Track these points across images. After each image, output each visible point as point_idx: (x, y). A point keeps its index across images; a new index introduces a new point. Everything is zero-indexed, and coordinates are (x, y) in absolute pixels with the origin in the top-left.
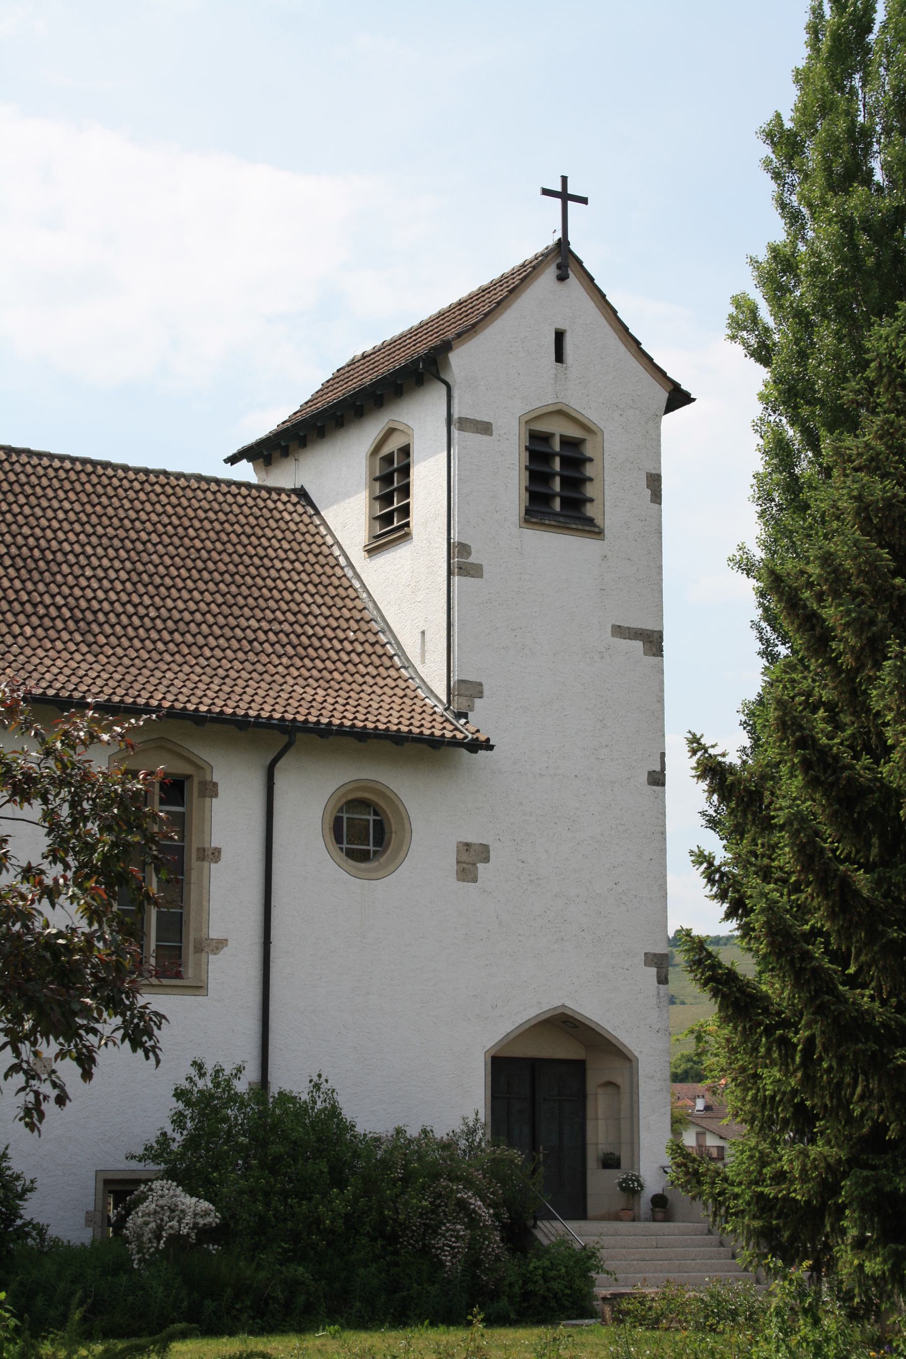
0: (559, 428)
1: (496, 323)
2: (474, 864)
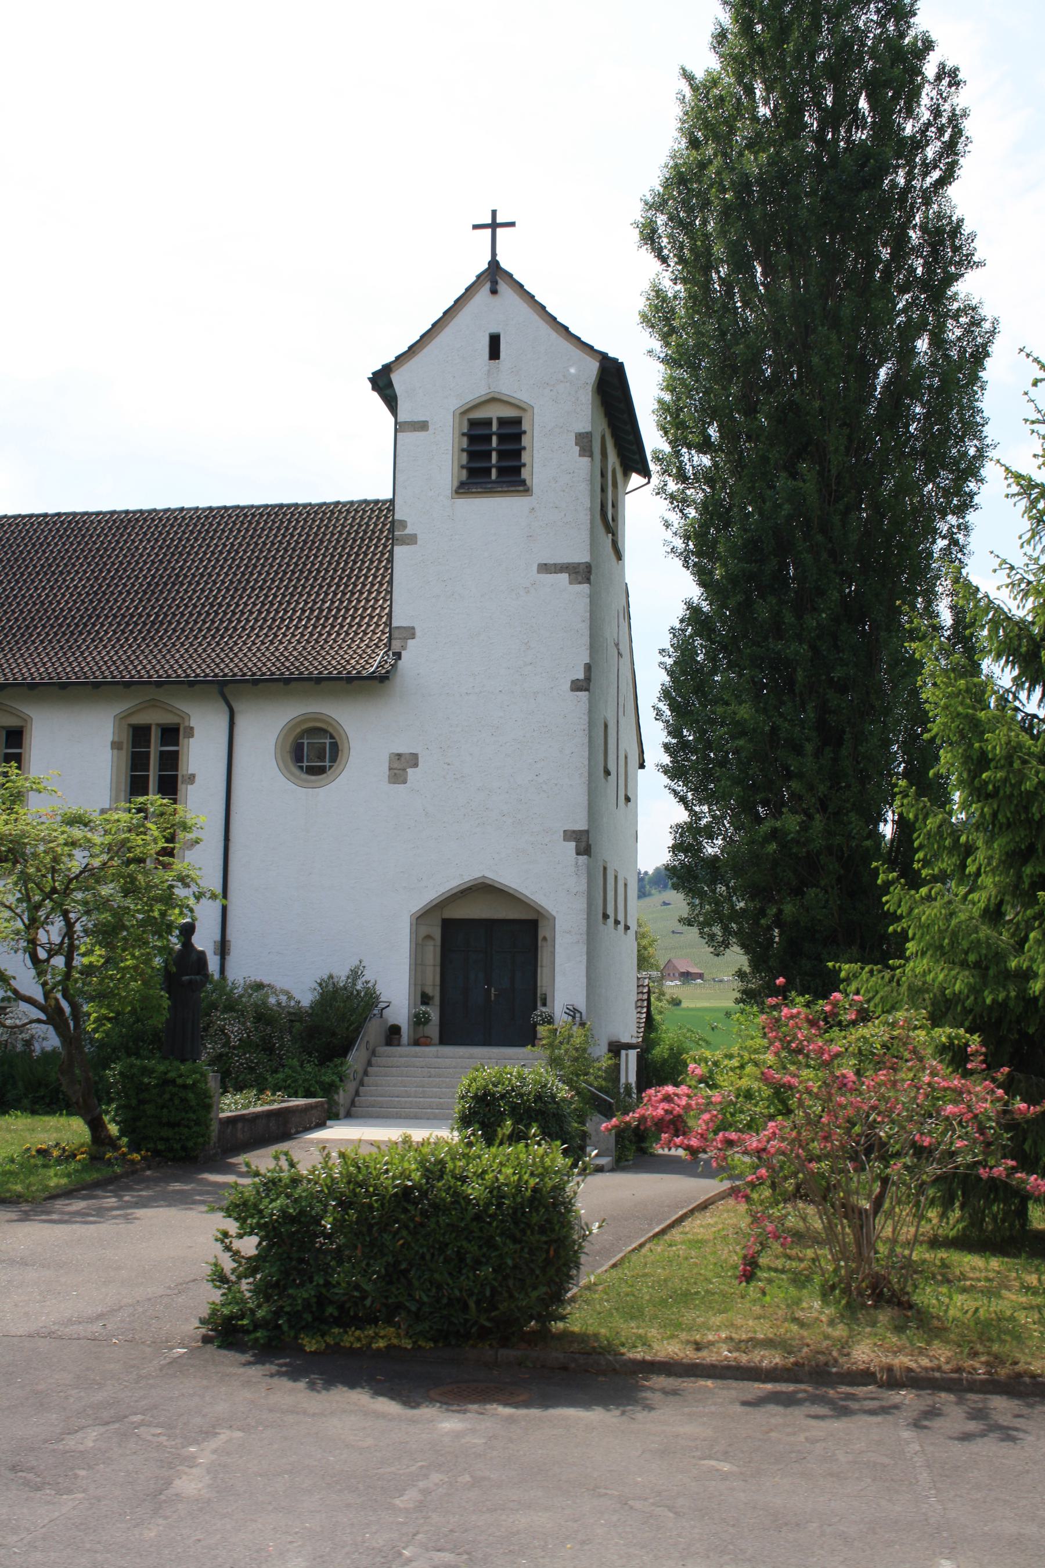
0: (494, 413)
1: (425, 350)
2: (404, 770)
